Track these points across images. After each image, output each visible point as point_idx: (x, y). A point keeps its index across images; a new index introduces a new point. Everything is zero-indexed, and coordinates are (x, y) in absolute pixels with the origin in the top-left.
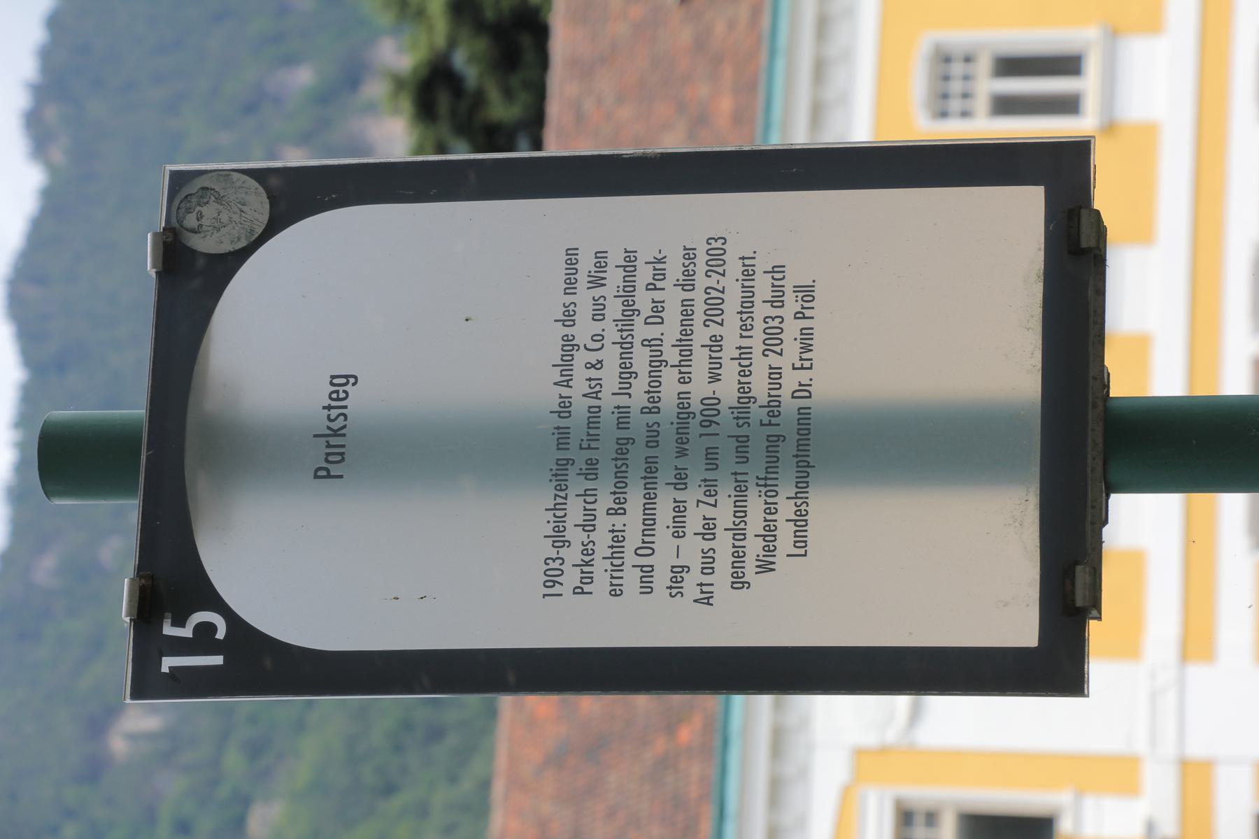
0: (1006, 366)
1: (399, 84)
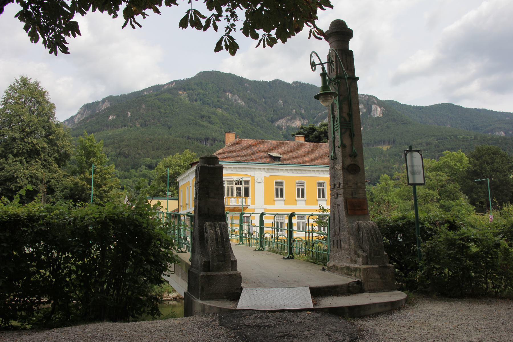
0: (417, 182)
1: (313, 126)
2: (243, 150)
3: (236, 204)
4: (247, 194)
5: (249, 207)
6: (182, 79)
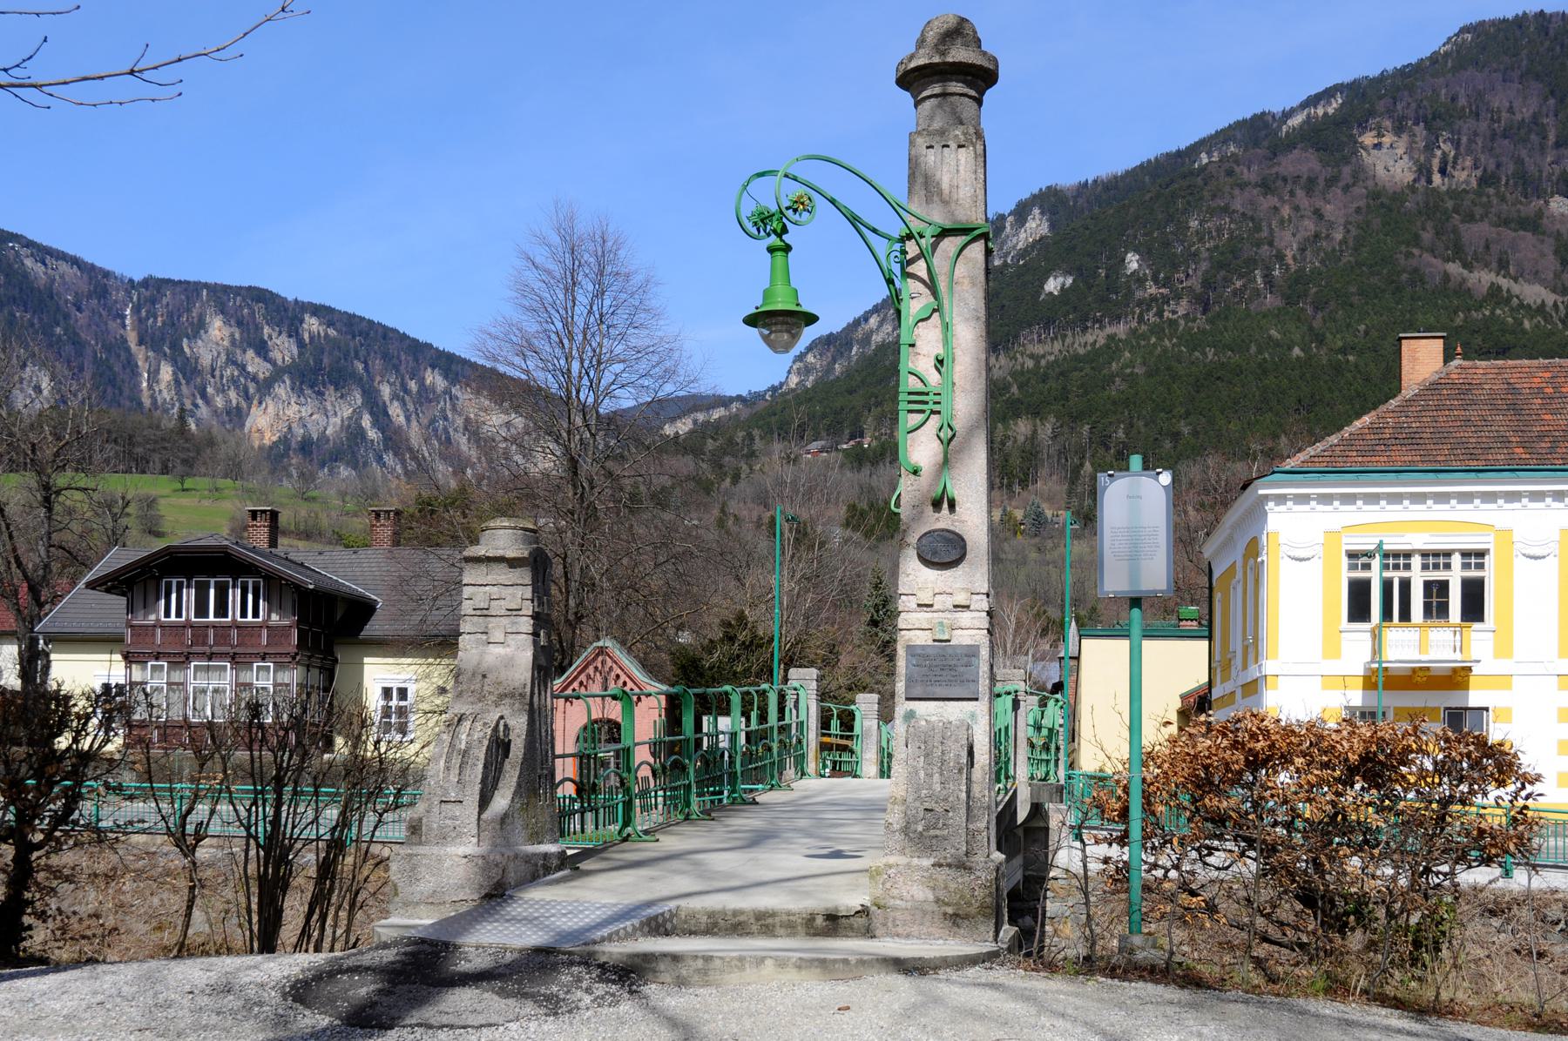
2: (1473, 414)
3: (1416, 657)
4: (1474, 607)
5: (1476, 670)
6: (1374, 72)
